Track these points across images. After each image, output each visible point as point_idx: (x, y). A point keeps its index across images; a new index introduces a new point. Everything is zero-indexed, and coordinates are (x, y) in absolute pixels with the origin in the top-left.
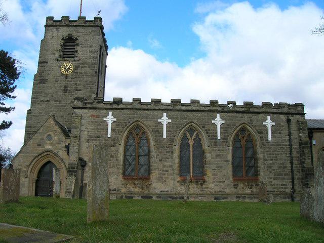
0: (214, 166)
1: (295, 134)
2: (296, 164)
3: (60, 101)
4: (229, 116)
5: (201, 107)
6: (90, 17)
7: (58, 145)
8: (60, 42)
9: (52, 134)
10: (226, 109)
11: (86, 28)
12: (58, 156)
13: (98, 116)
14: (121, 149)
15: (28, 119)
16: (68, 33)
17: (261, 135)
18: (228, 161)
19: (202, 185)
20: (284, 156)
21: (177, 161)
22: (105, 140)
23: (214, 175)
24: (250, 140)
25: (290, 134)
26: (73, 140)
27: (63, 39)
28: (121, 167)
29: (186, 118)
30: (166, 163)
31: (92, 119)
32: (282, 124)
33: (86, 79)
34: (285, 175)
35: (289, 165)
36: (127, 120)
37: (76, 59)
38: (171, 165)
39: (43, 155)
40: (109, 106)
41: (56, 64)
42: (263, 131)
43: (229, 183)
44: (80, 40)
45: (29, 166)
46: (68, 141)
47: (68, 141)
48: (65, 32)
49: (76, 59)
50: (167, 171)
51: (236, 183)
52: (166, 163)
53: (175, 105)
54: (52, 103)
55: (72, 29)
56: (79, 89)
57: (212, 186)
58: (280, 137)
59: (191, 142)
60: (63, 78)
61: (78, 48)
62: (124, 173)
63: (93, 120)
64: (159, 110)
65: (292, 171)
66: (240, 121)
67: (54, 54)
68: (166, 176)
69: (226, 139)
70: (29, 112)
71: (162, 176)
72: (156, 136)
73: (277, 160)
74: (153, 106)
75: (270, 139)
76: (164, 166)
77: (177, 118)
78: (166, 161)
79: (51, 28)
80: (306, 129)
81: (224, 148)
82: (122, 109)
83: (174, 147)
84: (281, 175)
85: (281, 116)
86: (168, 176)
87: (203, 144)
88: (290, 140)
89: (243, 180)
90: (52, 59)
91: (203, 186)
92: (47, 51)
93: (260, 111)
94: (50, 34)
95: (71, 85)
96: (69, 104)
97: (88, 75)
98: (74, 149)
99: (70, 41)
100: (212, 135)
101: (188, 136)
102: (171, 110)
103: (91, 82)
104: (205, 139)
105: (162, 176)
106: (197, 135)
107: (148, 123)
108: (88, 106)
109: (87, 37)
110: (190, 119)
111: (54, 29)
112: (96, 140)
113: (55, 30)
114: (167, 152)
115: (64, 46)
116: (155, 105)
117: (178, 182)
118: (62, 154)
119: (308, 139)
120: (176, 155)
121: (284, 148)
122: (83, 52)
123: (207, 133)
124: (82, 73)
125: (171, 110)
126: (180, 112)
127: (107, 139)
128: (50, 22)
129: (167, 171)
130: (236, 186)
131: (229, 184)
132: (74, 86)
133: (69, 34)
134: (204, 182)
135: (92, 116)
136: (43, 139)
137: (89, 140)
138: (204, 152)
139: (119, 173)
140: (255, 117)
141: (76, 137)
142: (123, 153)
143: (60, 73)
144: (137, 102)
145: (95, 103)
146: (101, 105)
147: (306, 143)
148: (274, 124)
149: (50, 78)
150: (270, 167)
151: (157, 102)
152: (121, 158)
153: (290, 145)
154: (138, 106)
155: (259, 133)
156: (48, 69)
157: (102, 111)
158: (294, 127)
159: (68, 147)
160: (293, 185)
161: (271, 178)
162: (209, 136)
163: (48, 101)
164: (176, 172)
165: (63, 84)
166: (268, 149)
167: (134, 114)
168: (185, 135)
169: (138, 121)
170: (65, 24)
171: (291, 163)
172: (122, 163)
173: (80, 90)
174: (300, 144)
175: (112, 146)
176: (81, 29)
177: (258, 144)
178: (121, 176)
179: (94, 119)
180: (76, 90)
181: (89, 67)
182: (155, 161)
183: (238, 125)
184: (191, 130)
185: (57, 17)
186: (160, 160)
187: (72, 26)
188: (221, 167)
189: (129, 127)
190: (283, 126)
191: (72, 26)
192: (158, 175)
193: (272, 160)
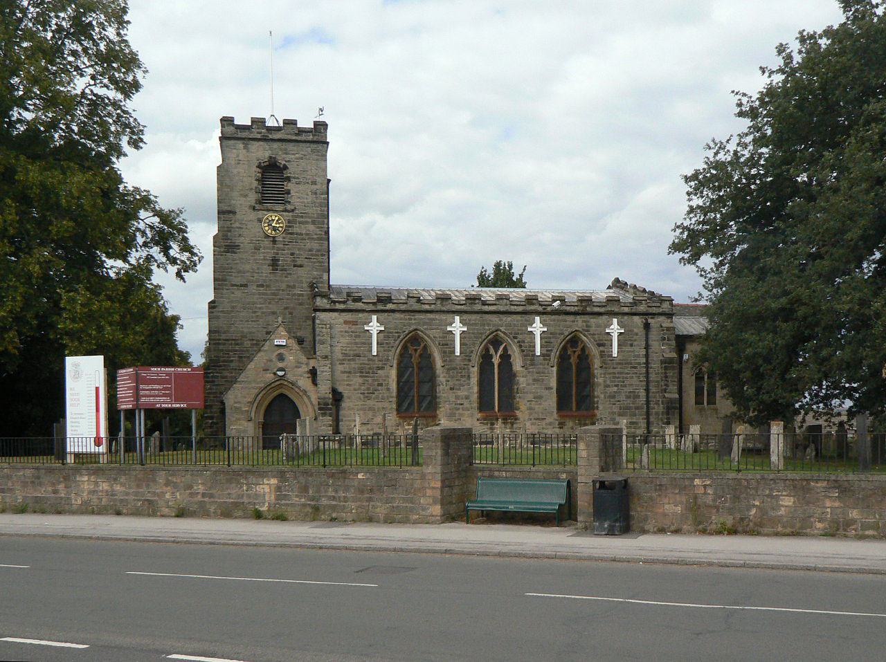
0: (530, 397)
1: (655, 345)
2: (653, 393)
3: (267, 286)
4: (554, 320)
5: (512, 307)
6: (306, 122)
7: (296, 369)
8: (255, 172)
9: (285, 352)
10: (549, 309)
11: (301, 144)
12: (299, 388)
13: (355, 323)
14: (393, 373)
15: (212, 318)
16: (267, 154)
17: (602, 348)
18: (551, 388)
19: (512, 424)
20: (635, 381)
21: (476, 389)
22: (369, 360)
23: (530, 409)
24: (584, 357)
25: (647, 347)
26: (323, 362)
27: (259, 167)
28: (394, 399)
29: (489, 325)
30: (459, 393)
31: (346, 328)
32: (635, 330)
33: (309, 245)
34: (637, 408)
35: (643, 393)
36: (401, 329)
37: (289, 207)
38: (469, 396)
39: (273, 385)
40: (371, 307)
41: (253, 215)
42: (604, 342)
43: (552, 420)
44: (293, 170)
45: (252, 403)
46: (312, 363)
47: (312, 363)
48: (262, 152)
49: (289, 207)
50: (462, 404)
51: (562, 421)
52: (459, 393)
53: (472, 304)
54: (253, 288)
55: (276, 145)
56: (299, 263)
57: (527, 424)
58: (630, 351)
59: (496, 360)
60: (267, 243)
61: (289, 186)
62: (398, 410)
63: (347, 329)
64: (448, 312)
65: (648, 402)
66: (570, 327)
67: (246, 196)
68: (461, 411)
69: (549, 356)
70: (212, 305)
71: (454, 411)
72: (445, 352)
73: (625, 386)
74: (439, 307)
75: (615, 354)
76: (457, 397)
77: (476, 324)
78: (459, 389)
79: (232, 142)
80: (673, 337)
81: (544, 368)
82: (393, 311)
83: (472, 369)
84: (629, 408)
85: (634, 317)
86: (464, 412)
87: (514, 363)
88: (647, 356)
89: (573, 416)
90: (243, 202)
91: (515, 426)
92: (232, 190)
93: (602, 310)
94: (232, 155)
95: (284, 259)
96: (283, 290)
97: (313, 238)
98: (324, 372)
99: (272, 172)
100: (528, 352)
101: (492, 351)
102: (466, 312)
103: (318, 251)
104: (516, 354)
105: (454, 411)
106: (505, 349)
107: (432, 333)
108: (338, 306)
109: (303, 163)
110: (494, 325)
111: (240, 145)
112: (354, 360)
113: (241, 146)
114: (462, 376)
115: (261, 181)
116: (441, 304)
117: (478, 420)
118: (305, 383)
119: (674, 355)
120: (474, 380)
121: (635, 368)
122: (299, 194)
123: (521, 346)
124: (301, 234)
125: (466, 312)
126: (480, 315)
127: (372, 359)
128: (230, 129)
129: (462, 404)
130: (561, 425)
131: (551, 422)
132: (289, 259)
133: (270, 157)
134: (516, 419)
135: (346, 322)
136: (271, 361)
137: (343, 360)
138: (515, 375)
139: (392, 408)
140: (593, 321)
141: (326, 357)
142: (396, 379)
143: (262, 234)
144: (415, 300)
145: (350, 302)
146: (359, 305)
147: (670, 361)
148: (623, 331)
149: (244, 242)
150: (614, 397)
151: (444, 298)
152: (394, 386)
153: (647, 363)
154: (417, 307)
155: (599, 345)
156: (237, 225)
157: (361, 315)
158: (654, 335)
159: (313, 373)
160: (648, 424)
161: (614, 413)
162: (523, 351)
163: (246, 286)
164: (475, 405)
165: (270, 254)
166: (611, 371)
167: (410, 319)
168: (487, 350)
169: (416, 329)
170: (259, 136)
171: (647, 390)
172: (394, 394)
173: (301, 266)
174: (662, 362)
175: (379, 368)
176: (291, 147)
177: (597, 363)
178: (395, 413)
179: (349, 328)
180: (295, 266)
181: (313, 223)
182: (444, 390)
183: (567, 333)
184: (496, 342)
185: (243, 119)
186: (451, 389)
187: (273, 140)
188: (540, 397)
189: (404, 340)
190: (637, 334)
191: (273, 140)
192: (448, 411)
193: (616, 386)
